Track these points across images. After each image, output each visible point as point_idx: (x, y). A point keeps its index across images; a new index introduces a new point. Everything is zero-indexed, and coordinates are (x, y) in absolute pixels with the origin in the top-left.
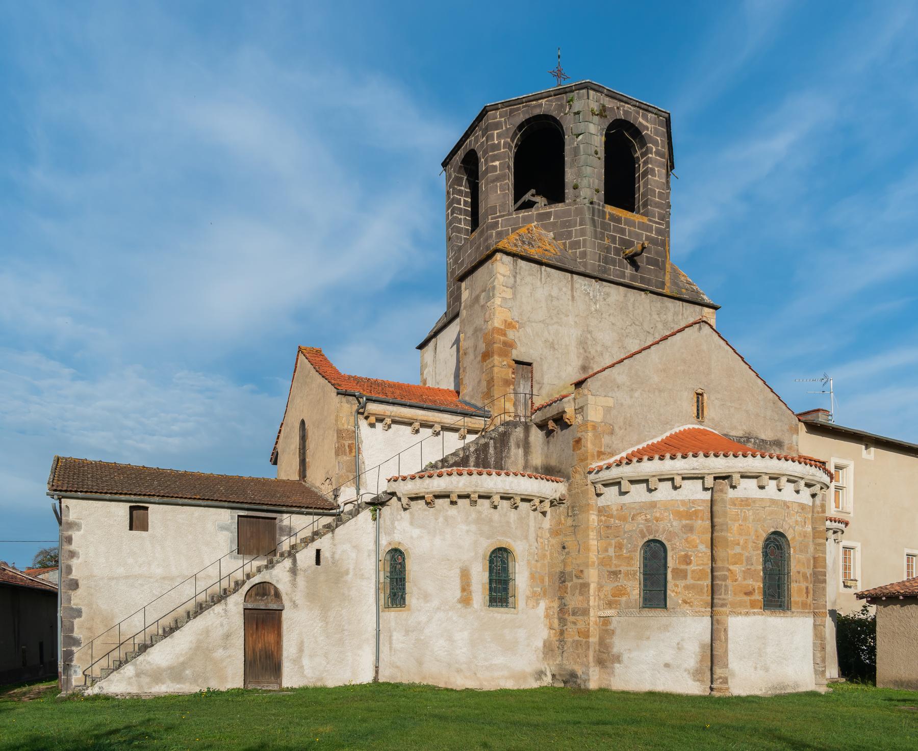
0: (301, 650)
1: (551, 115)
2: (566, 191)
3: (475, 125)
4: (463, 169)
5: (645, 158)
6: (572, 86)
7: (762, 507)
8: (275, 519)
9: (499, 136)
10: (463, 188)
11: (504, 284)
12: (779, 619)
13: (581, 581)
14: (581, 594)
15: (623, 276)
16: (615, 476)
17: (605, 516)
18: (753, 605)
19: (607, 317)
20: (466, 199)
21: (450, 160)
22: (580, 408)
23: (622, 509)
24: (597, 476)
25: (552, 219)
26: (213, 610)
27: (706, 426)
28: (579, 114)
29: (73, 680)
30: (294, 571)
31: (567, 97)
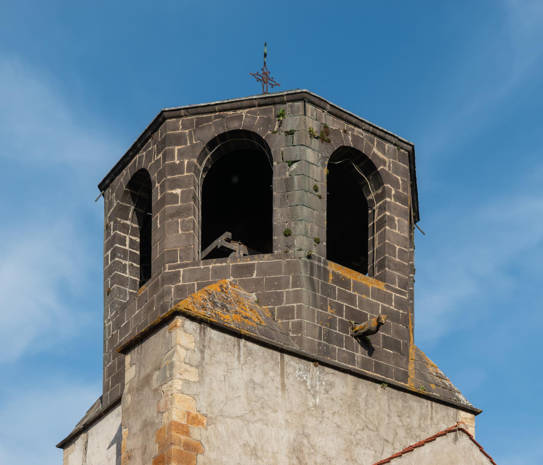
1: (253, 132)
2: (275, 238)
3: (147, 135)
4: (129, 195)
5: (381, 203)
6: (282, 96)
9: (181, 154)
10: (128, 222)
11: (187, 361)
15: (352, 360)
19: (330, 416)
20: (134, 238)
25: (255, 274)
28: (293, 134)
31: (276, 110)
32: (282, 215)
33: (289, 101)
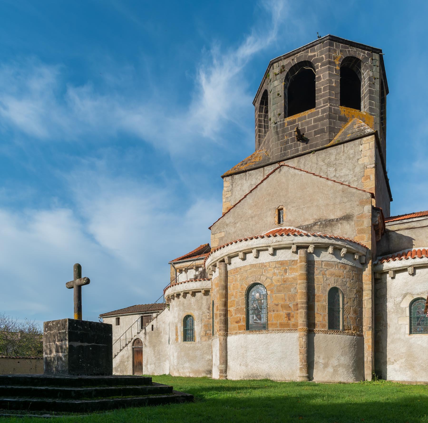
0: (147, 362)
7: (246, 271)
8: (151, 316)
12: (255, 335)
18: (240, 328)
27: (284, 226)
30: (145, 334)
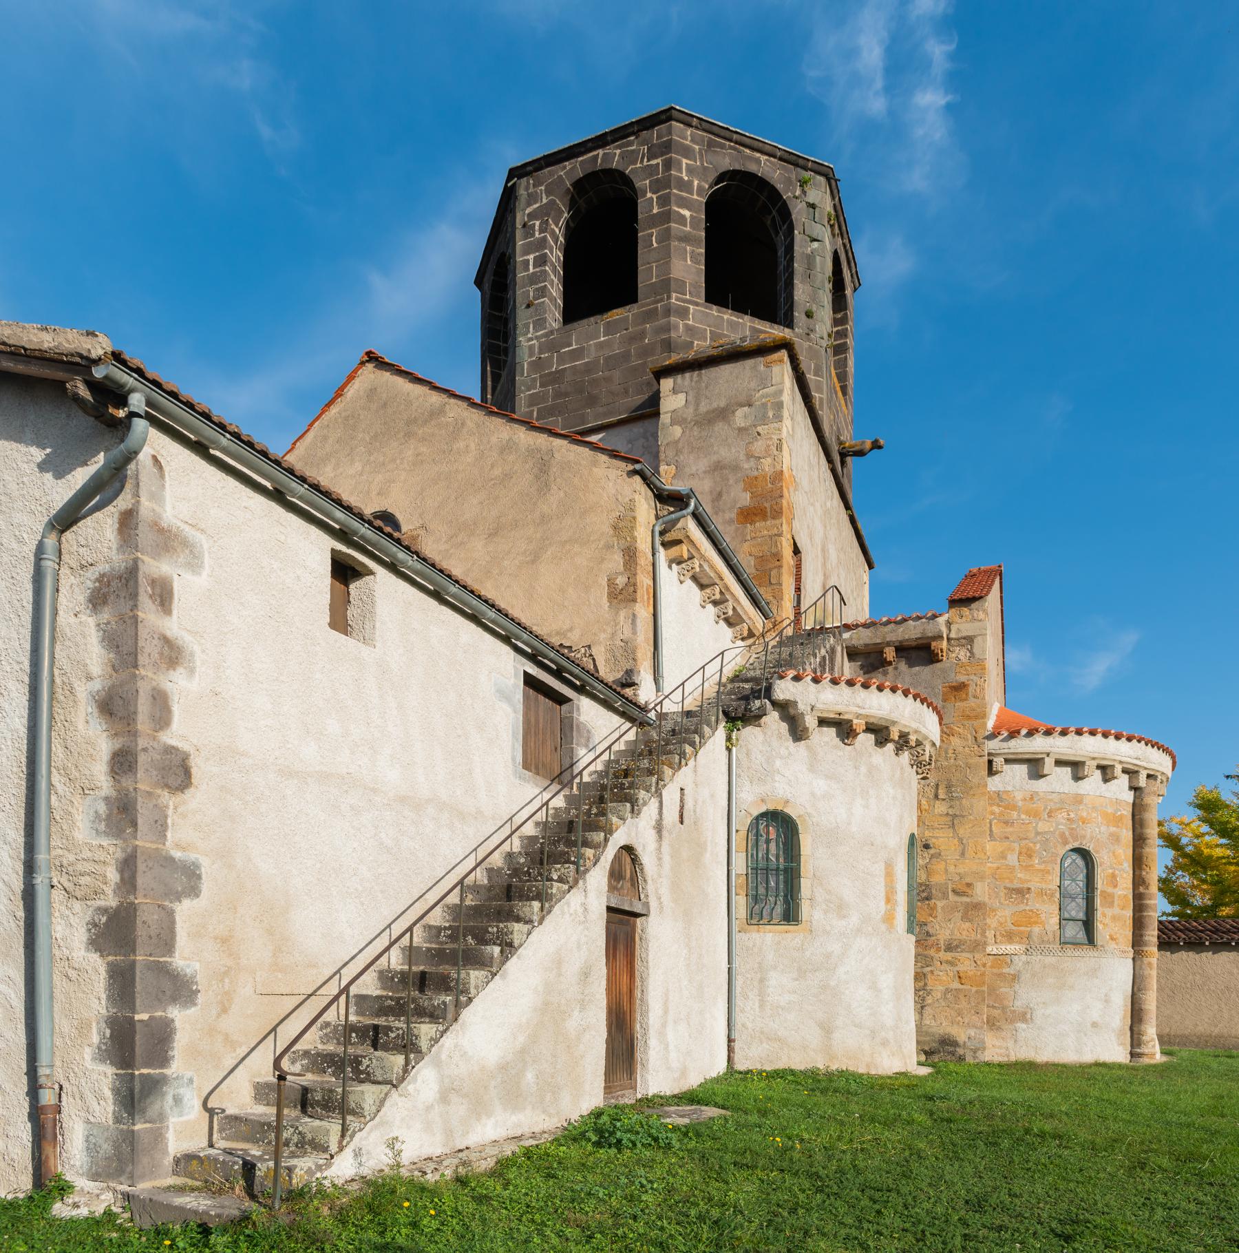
0: (666, 1012)
4: (569, 197)
5: (840, 328)
6: (808, 160)
8: (561, 700)
13: (965, 899)
14: (965, 918)
16: (1038, 750)
17: (1000, 806)
21: (537, 170)
22: (964, 638)
23: (1032, 798)
24: (1005, 745)
26: (568, 904)
29: (171, 1136)
30: (659, 828)
32: (803, 292)
33: (811, 170)
